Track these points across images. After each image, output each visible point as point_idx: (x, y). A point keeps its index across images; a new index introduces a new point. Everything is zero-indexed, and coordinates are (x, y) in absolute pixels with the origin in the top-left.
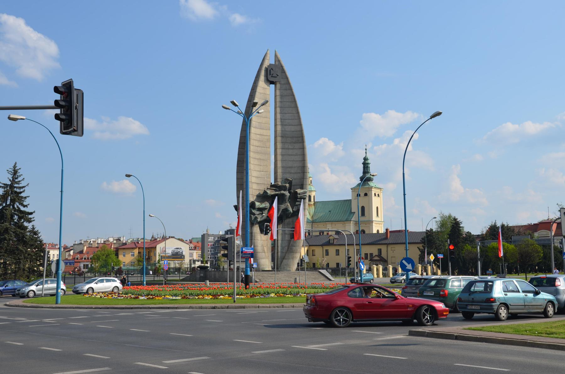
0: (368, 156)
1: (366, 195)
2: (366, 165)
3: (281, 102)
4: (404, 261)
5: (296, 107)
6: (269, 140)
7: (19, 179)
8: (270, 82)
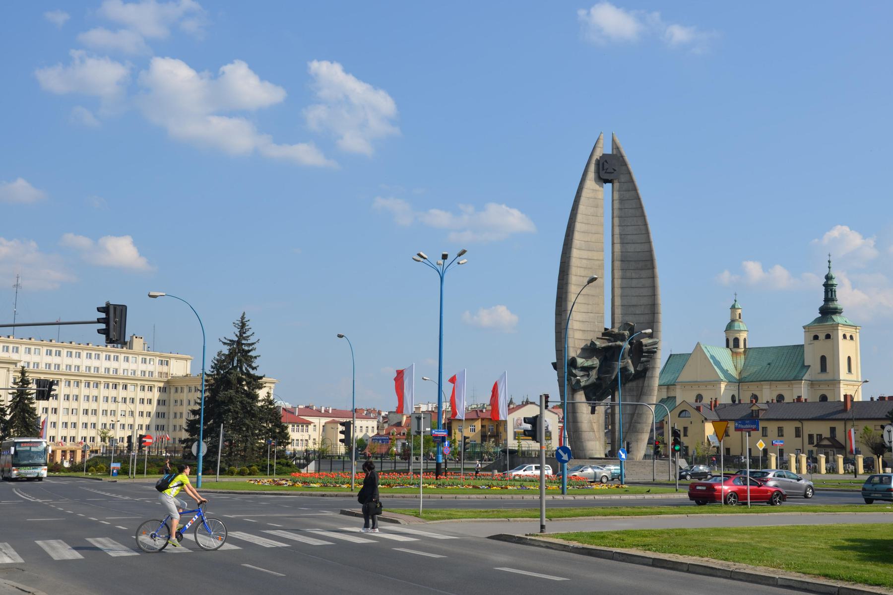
0: (834, 274)
1: (828, 337)
2: (829, 288)
3: (620, 209)
4: (560, 451)
5: (643, 216)
6: (601, 267)
7: (248, 334)
8: (602, 179)
